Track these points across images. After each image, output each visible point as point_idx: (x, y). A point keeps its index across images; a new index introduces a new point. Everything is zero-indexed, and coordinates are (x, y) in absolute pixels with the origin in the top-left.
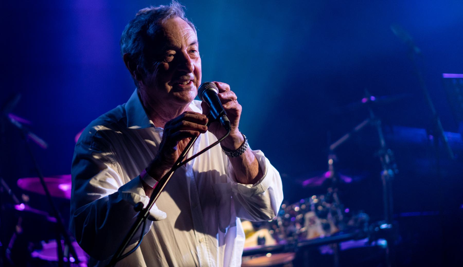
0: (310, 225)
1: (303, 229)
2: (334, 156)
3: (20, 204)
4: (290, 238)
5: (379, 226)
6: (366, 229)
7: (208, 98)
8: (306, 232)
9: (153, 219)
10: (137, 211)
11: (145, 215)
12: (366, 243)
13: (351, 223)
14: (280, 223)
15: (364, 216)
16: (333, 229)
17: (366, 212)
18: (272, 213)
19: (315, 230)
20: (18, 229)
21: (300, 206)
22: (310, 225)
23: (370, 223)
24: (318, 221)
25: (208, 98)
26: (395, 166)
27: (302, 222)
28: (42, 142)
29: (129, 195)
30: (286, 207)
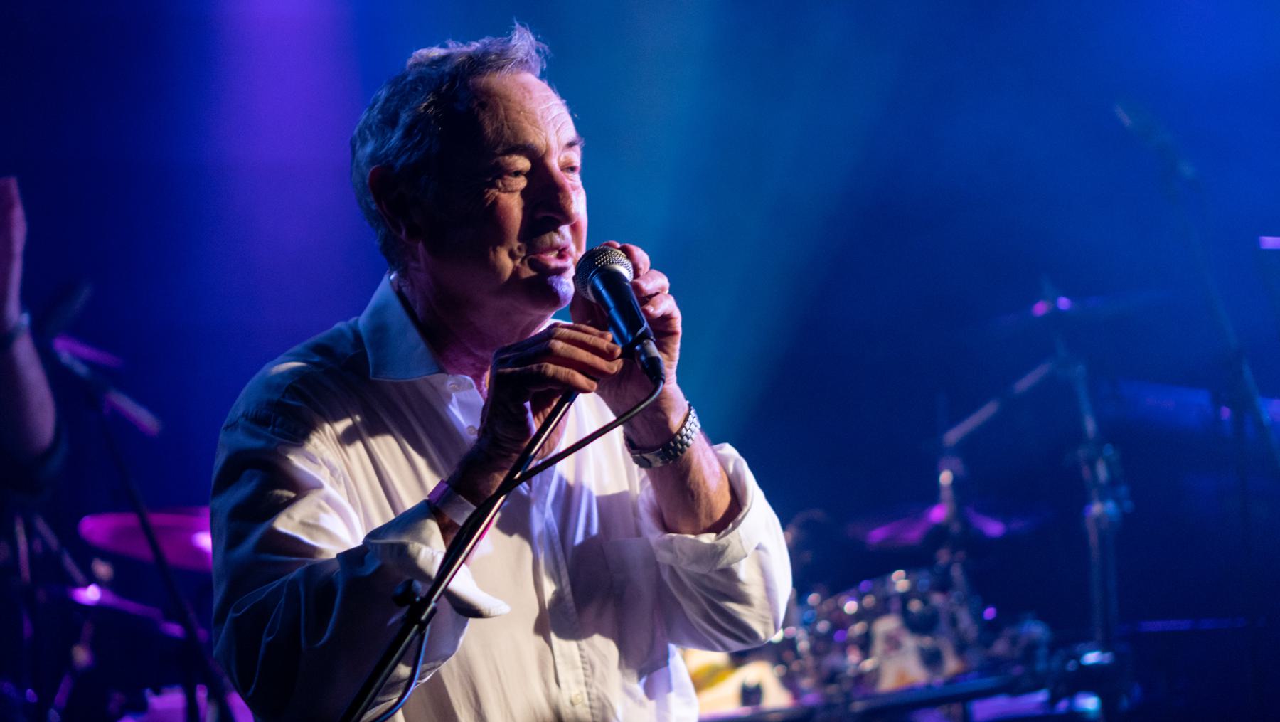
0: (886, 653)
1: (868, 665)
2: (956, 462)
3: (86, 586)
4: (832, 689)
5: (1077, 657)
6: (1041, 666)
7: (604, 292)
8: (876, 673)
9: (468, 611)
10: (402, 605)
11: (423, 617)
12: (1043, 705)
13: (1000, 647)
14: (803, 645)
15: (1036, 630)
16: (952, 665)
17: (1042, 617)
18: (765, 624)
19: (898, 666)
20: (81, 655)
21: (859, 598)
22: (886, 653)
23: (1053, 647)
24: (911, 643)
25: (604, 292)
26: (1123, 490)
27: (865, 645)
28: (145, 418)
29: (403, 549)
30: (821, 603)
